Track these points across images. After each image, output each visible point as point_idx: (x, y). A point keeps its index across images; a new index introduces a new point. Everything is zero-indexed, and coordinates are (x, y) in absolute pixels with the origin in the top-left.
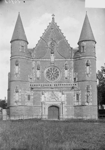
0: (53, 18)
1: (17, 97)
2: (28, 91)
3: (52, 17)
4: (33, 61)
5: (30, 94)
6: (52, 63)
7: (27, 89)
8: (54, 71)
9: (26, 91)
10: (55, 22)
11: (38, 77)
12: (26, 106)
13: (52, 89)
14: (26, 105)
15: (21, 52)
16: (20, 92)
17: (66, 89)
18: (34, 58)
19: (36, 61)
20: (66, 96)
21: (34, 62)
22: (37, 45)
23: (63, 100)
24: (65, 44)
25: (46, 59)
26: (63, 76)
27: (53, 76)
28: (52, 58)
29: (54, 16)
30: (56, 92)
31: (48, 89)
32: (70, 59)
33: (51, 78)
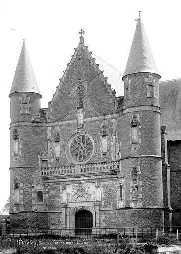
0: (80, 38)
1: (17, 197)
2: (38, 184)
3: (80, 35)
4: (47, 127)
5: (41, 190)
6: (79, 127)
7: (35, 182)
8: (83, 143)
9: (33, 185)
10: (86, 44)
11: (57, 156)
12: (34, 212)
13: (78, 177)
14: (33, 210)
15: (22, 114)
16: (21, 187)
17: (101, 177)
18: (49, 120)
19: (52, 127)
20: (103, 191)
21: (50, 129)
22: (54, 95)
23: (99, 199)
24: (104, 87)
25: (68, 120)
26: (98, 151)
27: (82, 154)
28: (81, 117)
29: (83, 32)
30: (109, 180)
31: (70, 179)
32: (110, 116)
33: (79, 155)
